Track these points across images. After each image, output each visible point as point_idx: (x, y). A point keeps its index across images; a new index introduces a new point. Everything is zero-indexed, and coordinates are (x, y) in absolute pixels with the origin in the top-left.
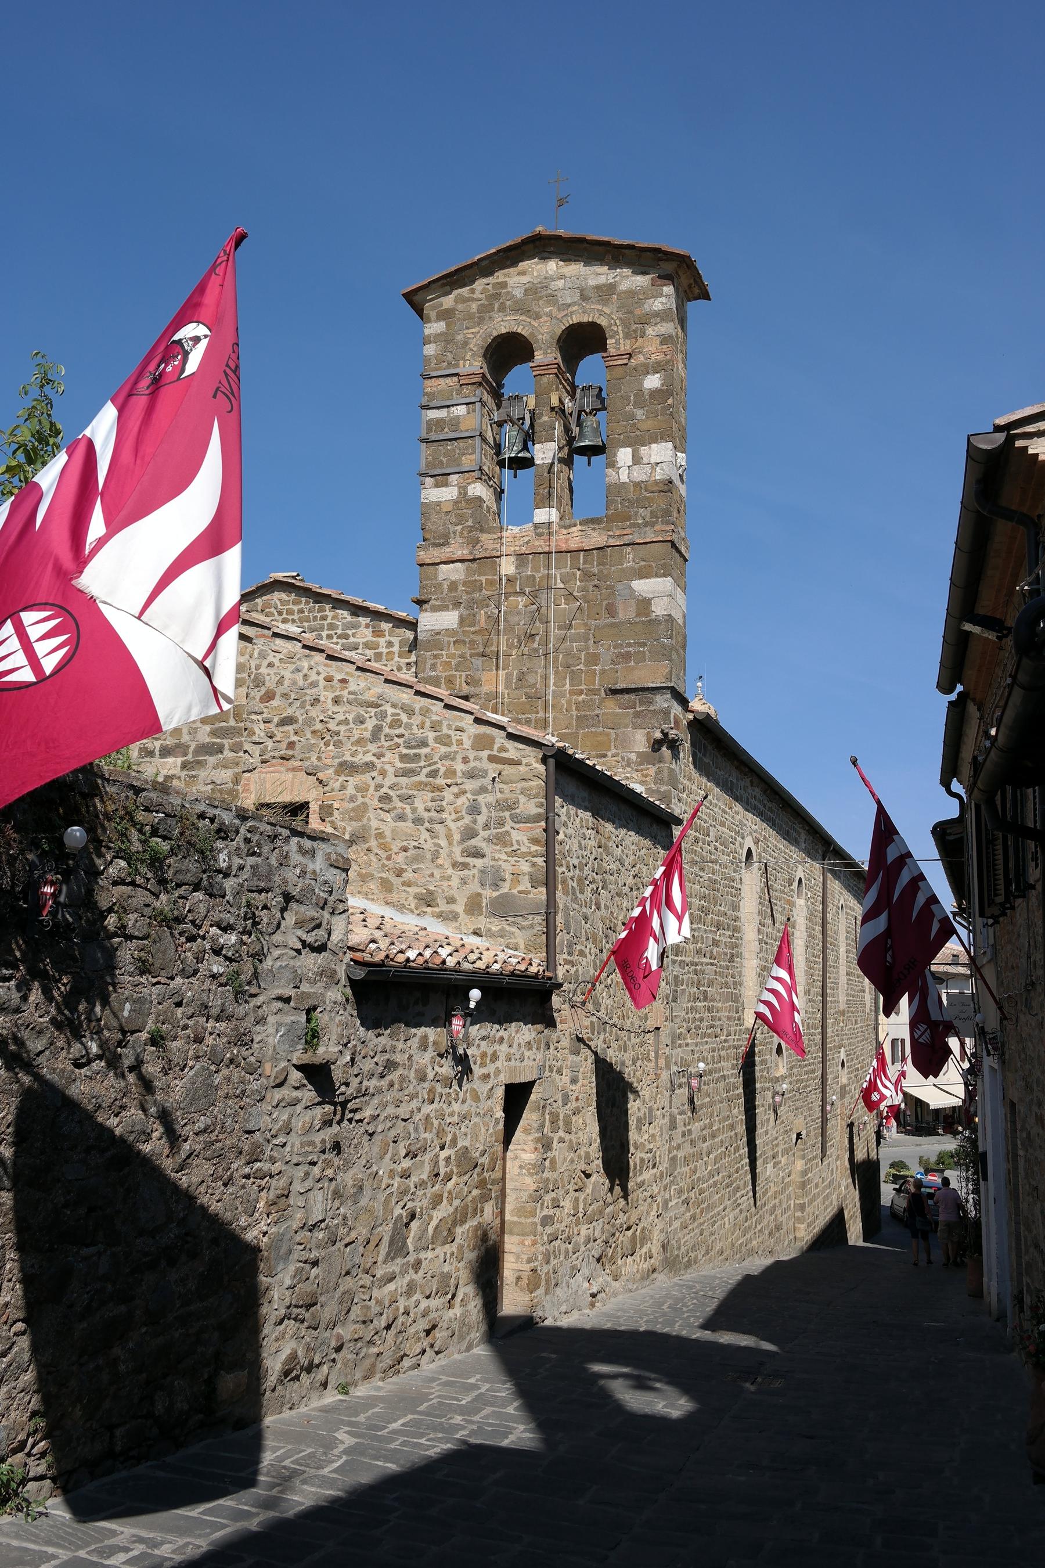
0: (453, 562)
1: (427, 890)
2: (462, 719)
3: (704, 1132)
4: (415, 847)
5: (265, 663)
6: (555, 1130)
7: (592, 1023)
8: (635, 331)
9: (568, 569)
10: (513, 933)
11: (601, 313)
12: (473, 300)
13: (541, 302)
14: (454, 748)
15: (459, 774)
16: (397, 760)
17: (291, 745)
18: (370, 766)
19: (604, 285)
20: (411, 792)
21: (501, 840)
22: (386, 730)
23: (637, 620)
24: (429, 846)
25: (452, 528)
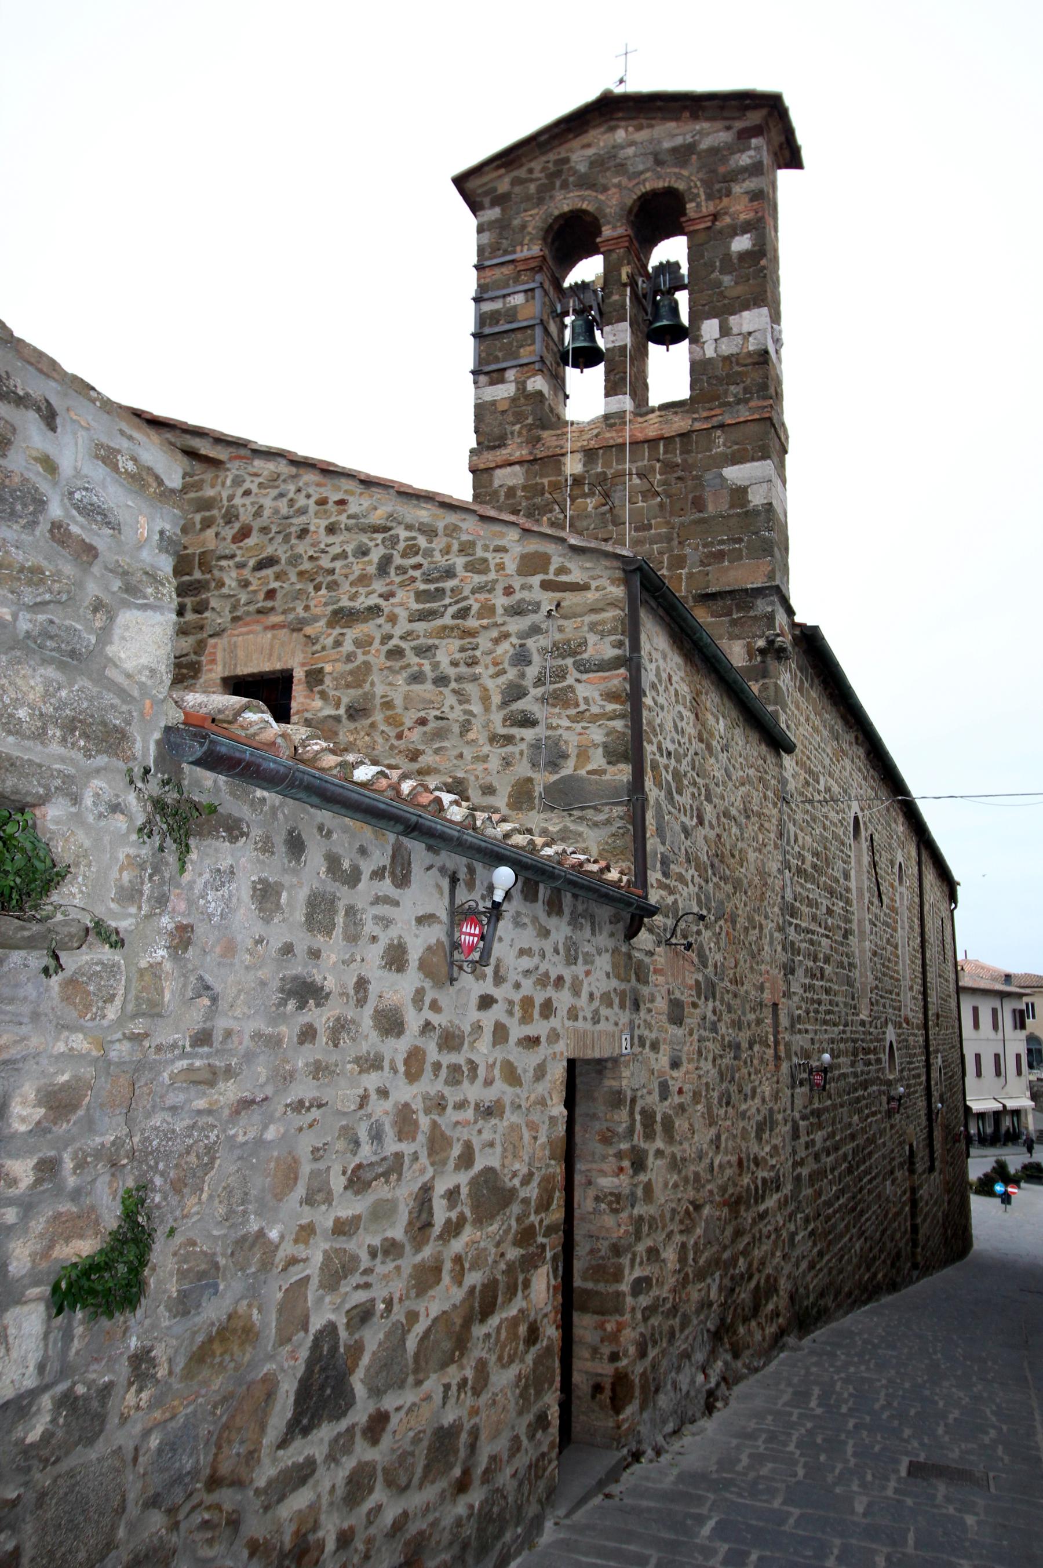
0: (510, 465)
1: (454, 778)
2: (502, 535)
3: (828, 1143)
4: (437, 718)
5: (240, 491)
6: (649, 1136)
7: (697, 982)
8: (719, 191)
9: (646, 462)
10: (580, 834)
11: (679, 177)
12: (532, 180)
13: (608, 174)
14: (492, 575)
15: (500, 611)
16: (412, 600)
17: (271, 594)
18: (375, 611)
19: (682, 146)
20: (430, 642)
21: (561, 699)
22: (398, 560)
23: (731, 512)
24: (456, 714)
25: (509, 428)
